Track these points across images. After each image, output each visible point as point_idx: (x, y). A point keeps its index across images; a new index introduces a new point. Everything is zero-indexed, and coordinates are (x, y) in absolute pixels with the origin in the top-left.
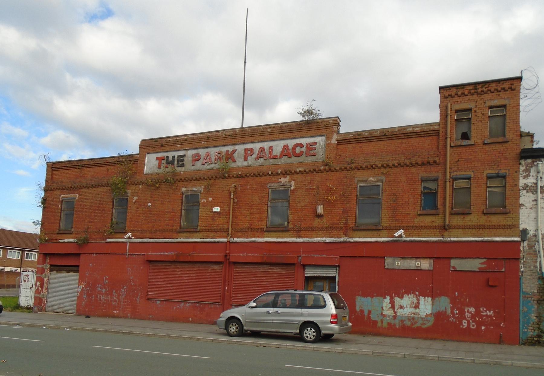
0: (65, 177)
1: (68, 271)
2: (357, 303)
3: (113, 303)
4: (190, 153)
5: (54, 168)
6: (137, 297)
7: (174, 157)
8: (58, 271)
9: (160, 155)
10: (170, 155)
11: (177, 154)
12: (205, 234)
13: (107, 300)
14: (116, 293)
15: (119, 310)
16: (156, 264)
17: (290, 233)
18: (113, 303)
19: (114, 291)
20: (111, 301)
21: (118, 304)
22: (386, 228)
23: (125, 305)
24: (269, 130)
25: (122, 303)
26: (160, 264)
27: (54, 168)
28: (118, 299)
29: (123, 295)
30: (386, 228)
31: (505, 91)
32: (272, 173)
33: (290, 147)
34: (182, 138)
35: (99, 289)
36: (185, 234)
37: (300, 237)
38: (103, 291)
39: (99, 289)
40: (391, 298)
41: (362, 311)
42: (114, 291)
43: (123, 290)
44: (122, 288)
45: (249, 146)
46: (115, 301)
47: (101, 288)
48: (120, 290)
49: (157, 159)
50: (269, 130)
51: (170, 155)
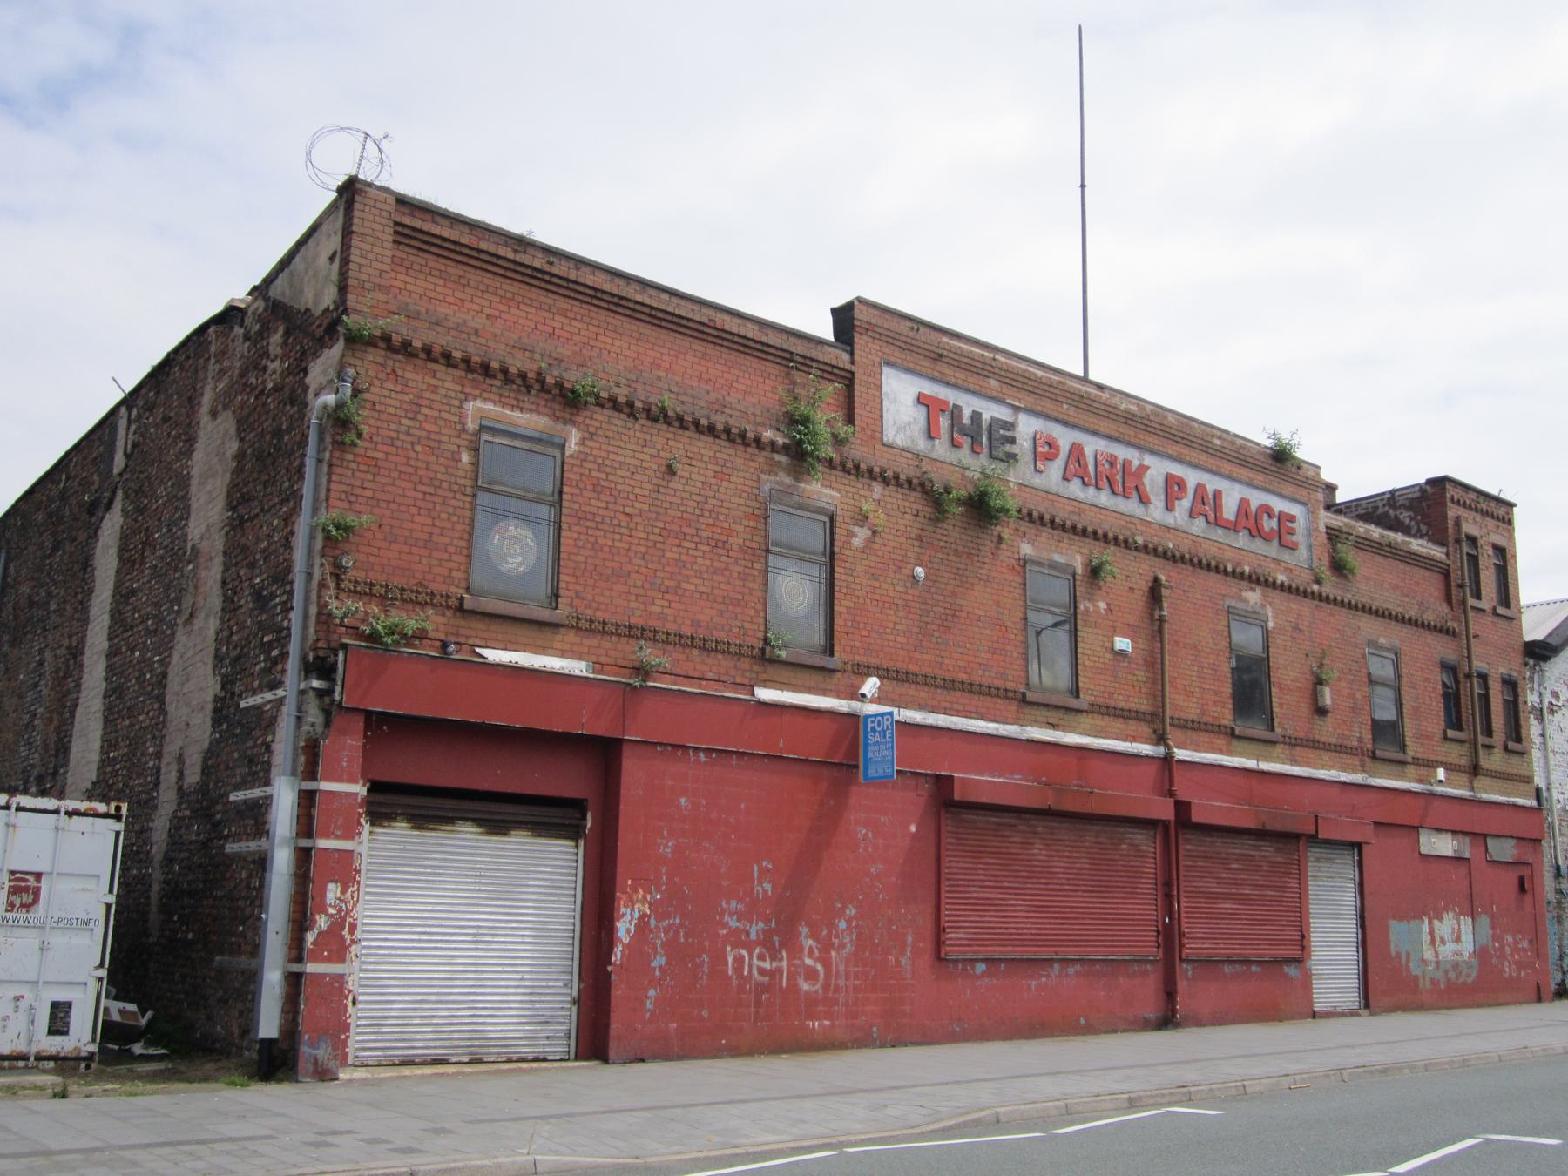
0: (393, 293)
1: (496, 826)
2: (1392, 938)
3: (805, 986)
4: (1027, 426)
5: (834, 311)
6: (903, 952)
7: (976, 416)
8: (421, 821)
9: (930, 388)
10: (969, 405)
11: (991, 412)
12: (1099, 721)
13: (774, 974)
14: (813, 935)
15: (829, 1016)
16: (969, 816)
17: (1279, 749)
18: (805, 986)
19: (804, 930)
20: (792, 977)
21: (826, 986)
22: (1417, 762)
23: (856, 989)
24: (1218, 442)
25: (842, 982)
26: (981, 819)
27: (834, 311)
28: (826, 963)
29: (843, 946)
30: (1417, 762)
31: (448, 365)
32: (1234, 571)
33: (1253, 508)
34: (1023, 366)
35: (734, 923)
36: (1045, 712)
37: (1294, 762)
38: (755, 929)
39: (734, 923)
40: (1430, 923)
41: (1398, 955)
42: (804, 930)
43: (843, 925)
44: (840, 914)
45: (1177, 470)
46: (811, 975)
47: (740, 916)
48: (831, 926)
49: (921, 400)
50: (1218, 442)
51: (969, 405)
